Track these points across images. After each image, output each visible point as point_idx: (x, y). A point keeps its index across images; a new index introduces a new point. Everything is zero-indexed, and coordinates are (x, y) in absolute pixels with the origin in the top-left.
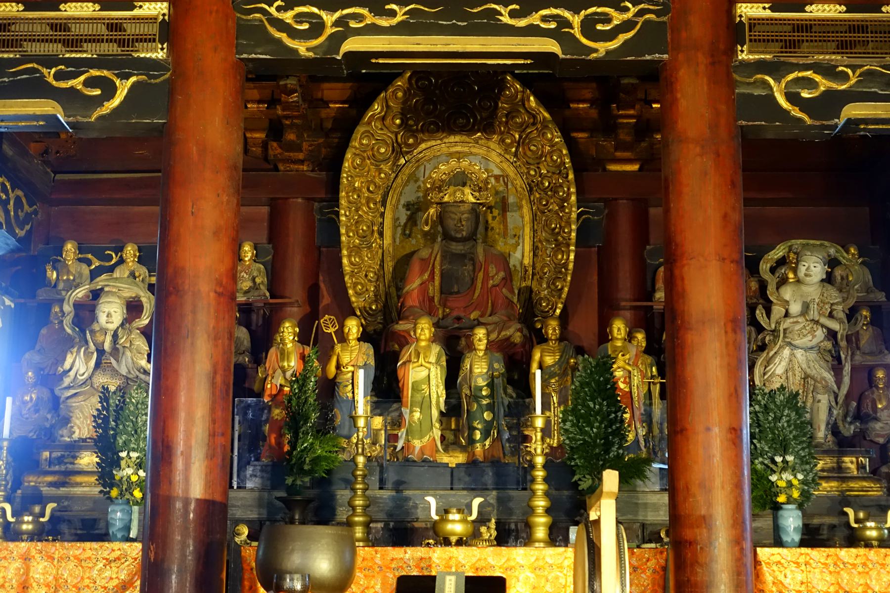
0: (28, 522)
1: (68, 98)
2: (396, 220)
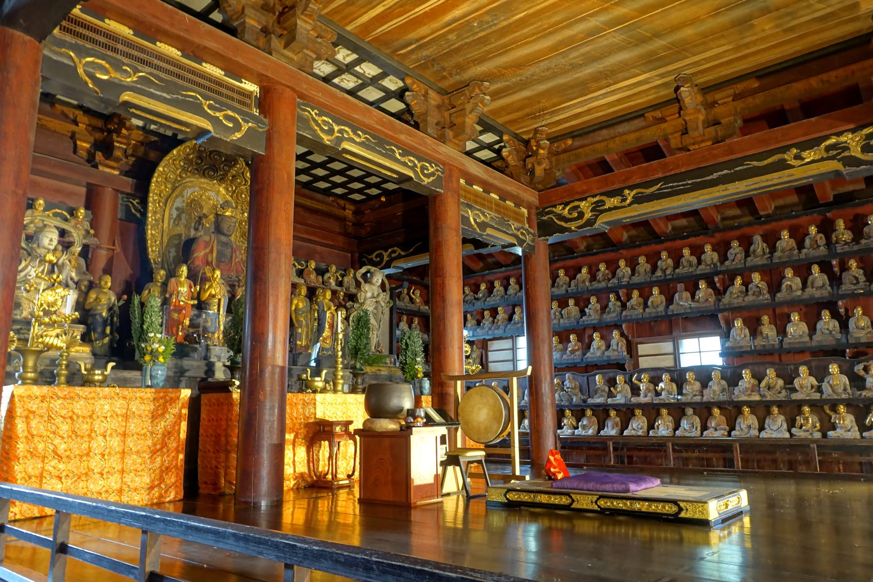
0: (98, 375)
1: (215, 121)
2: (170, 215)
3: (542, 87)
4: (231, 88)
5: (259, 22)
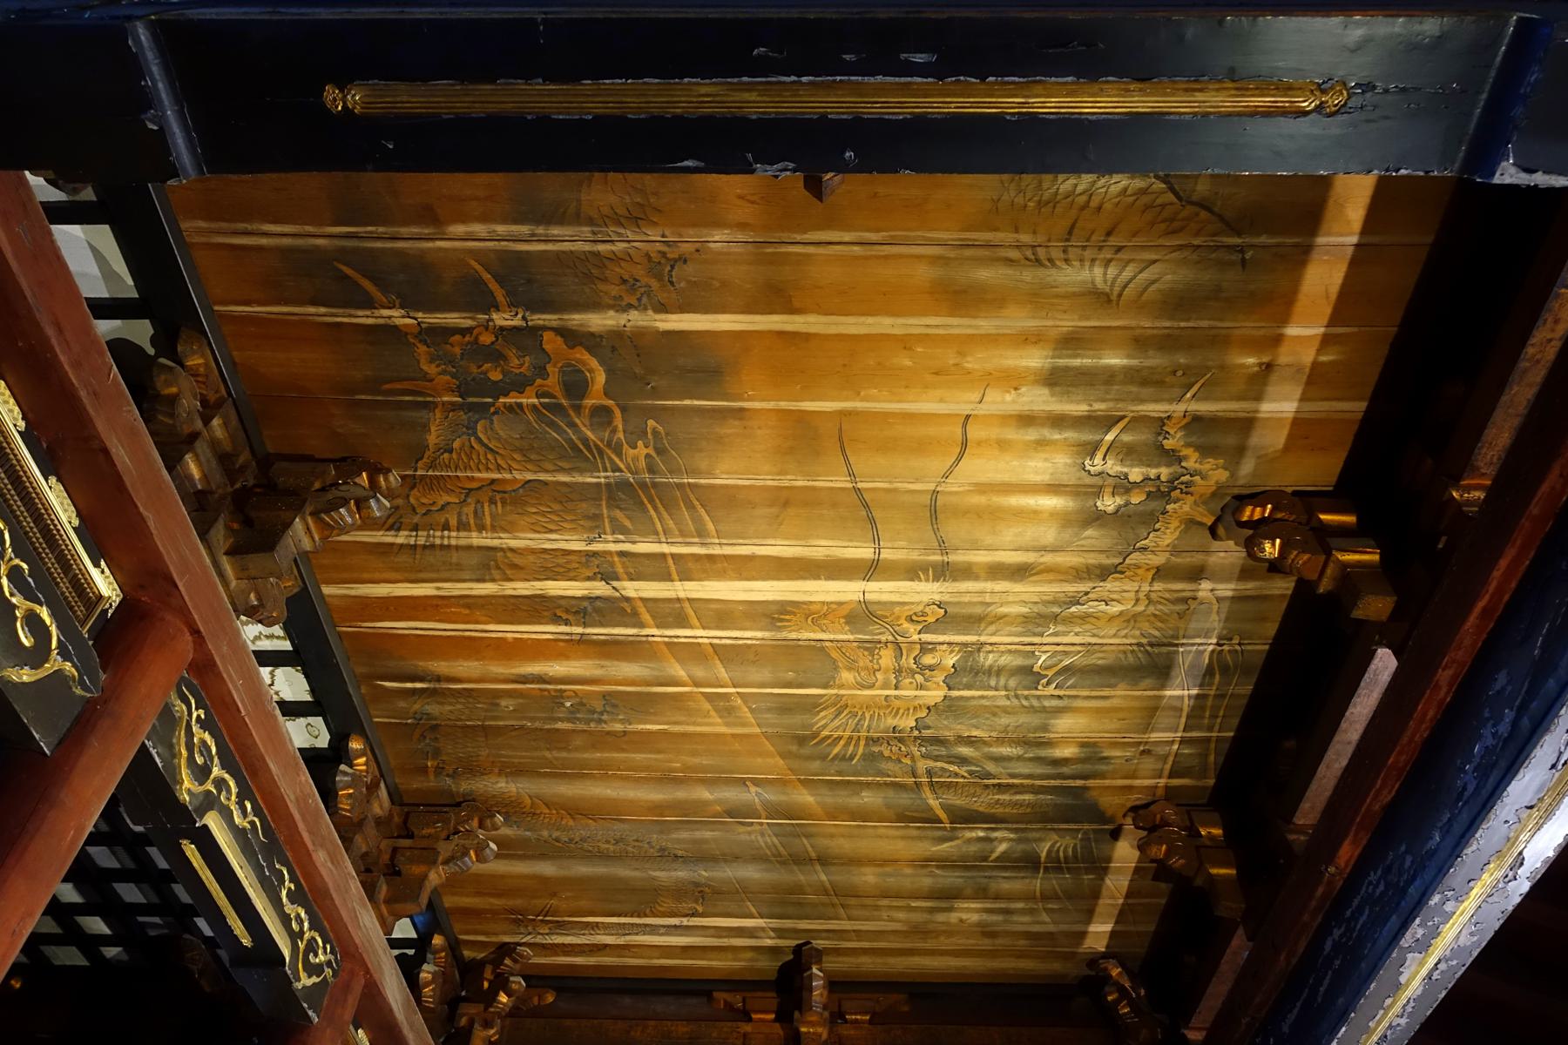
3: (583, 869)
4: (66, 562)
5: (205, 477)
